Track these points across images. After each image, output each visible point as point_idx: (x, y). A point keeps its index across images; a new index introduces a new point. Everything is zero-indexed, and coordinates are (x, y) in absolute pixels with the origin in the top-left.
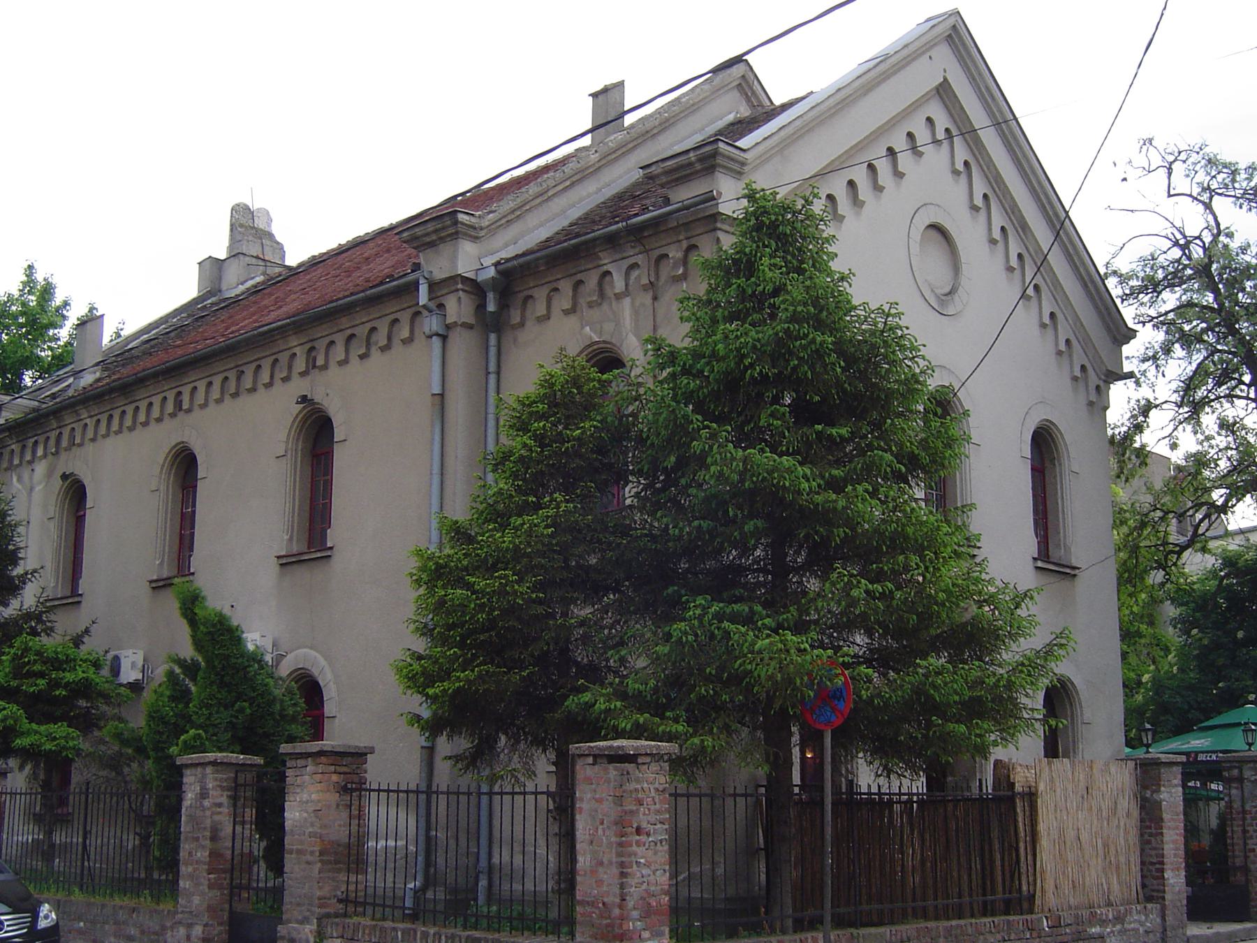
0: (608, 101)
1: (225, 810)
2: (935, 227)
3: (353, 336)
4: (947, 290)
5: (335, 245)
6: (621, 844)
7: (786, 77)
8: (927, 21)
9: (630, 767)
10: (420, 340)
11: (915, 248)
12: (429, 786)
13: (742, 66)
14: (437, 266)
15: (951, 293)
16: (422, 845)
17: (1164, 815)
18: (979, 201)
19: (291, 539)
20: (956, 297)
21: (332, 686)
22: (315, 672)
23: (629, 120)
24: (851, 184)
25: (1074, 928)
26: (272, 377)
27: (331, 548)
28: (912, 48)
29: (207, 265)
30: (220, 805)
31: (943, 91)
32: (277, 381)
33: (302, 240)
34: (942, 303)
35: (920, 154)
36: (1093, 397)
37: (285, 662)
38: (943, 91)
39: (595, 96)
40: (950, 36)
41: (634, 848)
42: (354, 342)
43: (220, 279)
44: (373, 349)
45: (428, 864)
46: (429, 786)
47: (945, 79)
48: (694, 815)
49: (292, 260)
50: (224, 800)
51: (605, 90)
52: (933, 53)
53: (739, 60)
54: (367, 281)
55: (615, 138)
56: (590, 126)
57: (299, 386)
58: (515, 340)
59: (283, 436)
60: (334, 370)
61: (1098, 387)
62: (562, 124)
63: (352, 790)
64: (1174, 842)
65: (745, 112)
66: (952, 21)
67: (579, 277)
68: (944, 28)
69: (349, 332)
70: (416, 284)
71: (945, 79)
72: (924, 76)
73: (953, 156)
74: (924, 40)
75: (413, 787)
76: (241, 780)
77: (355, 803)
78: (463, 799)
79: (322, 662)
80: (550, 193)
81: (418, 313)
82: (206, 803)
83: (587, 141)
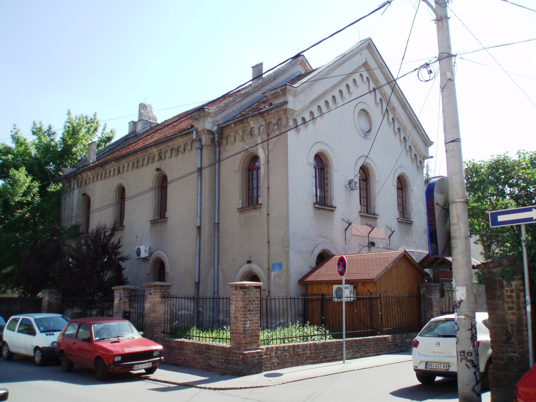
0: (258, 69)
1: (127, 304)
2: (363, 110)
3: (173, 149)
4: (368, 130)
5: (172, 117)
6: (244, 315)
7: (318, 60)
8: (360, 42)
9: (246, 290)
10: (194, 150)
11: (356, 117)
12: (198, 296)
13: (302, 57)
14: (199, 126)
15: (369, 131)
16: (196, 314)
17: (433, 303)
18: (378, 101)
19: (154, 215)
20: (371, 133)
21: (168, 263)
22: (162, 258)
23: (264, 76)
24: (334, 97)
25: (401, 340)
26: (148, 162)
27: (261, 204)
28: (354, 51)
29: (131, 124)
30: (125, 302)
31: (365, 65)
32: (150, 163)
33: (162, 114)
34: (366, 135)
35: (358, 86)
36: (419, 164)
37: (153, 255)
38: (365, 65)
39: (253, 67)
40: (368, 47)
41: (248, 315)
42: (173, 151)
43: (136, 128)
44: (179, 153)
45: (198, 320)
46: (198, 296)
47: (366, 61)
48: (281, 304)
49: (159, 121)
50: (127, 300)
51: (257, 66)
52: (362, 52)
53: (298, 55)
54: (179, 130)
55: (260, 81)
56: (252, 79)
57: (156, 165)
58: (225, 149)
59: (151, 181)
60: (167, 159)
61: (420, 161)
62: (245, 77)
63: (166, 297)
64: (437, 311)
65: (303, 72)
66: (368, 42)
67: (244, 129)
68: (366, 44)
69: (172, 147)
70: (192, 132)
71: (366, 61)
72: (358, 61)
73: (369, 87)
74: (358, 49)
75: (211, 297)
76: (132, 294)
77: (167, 301)
78: (281, 300)
79: (165, 255)
80: (236, 101)
81: (193, 141)
82: (121, 302)
83: (251, 82)
